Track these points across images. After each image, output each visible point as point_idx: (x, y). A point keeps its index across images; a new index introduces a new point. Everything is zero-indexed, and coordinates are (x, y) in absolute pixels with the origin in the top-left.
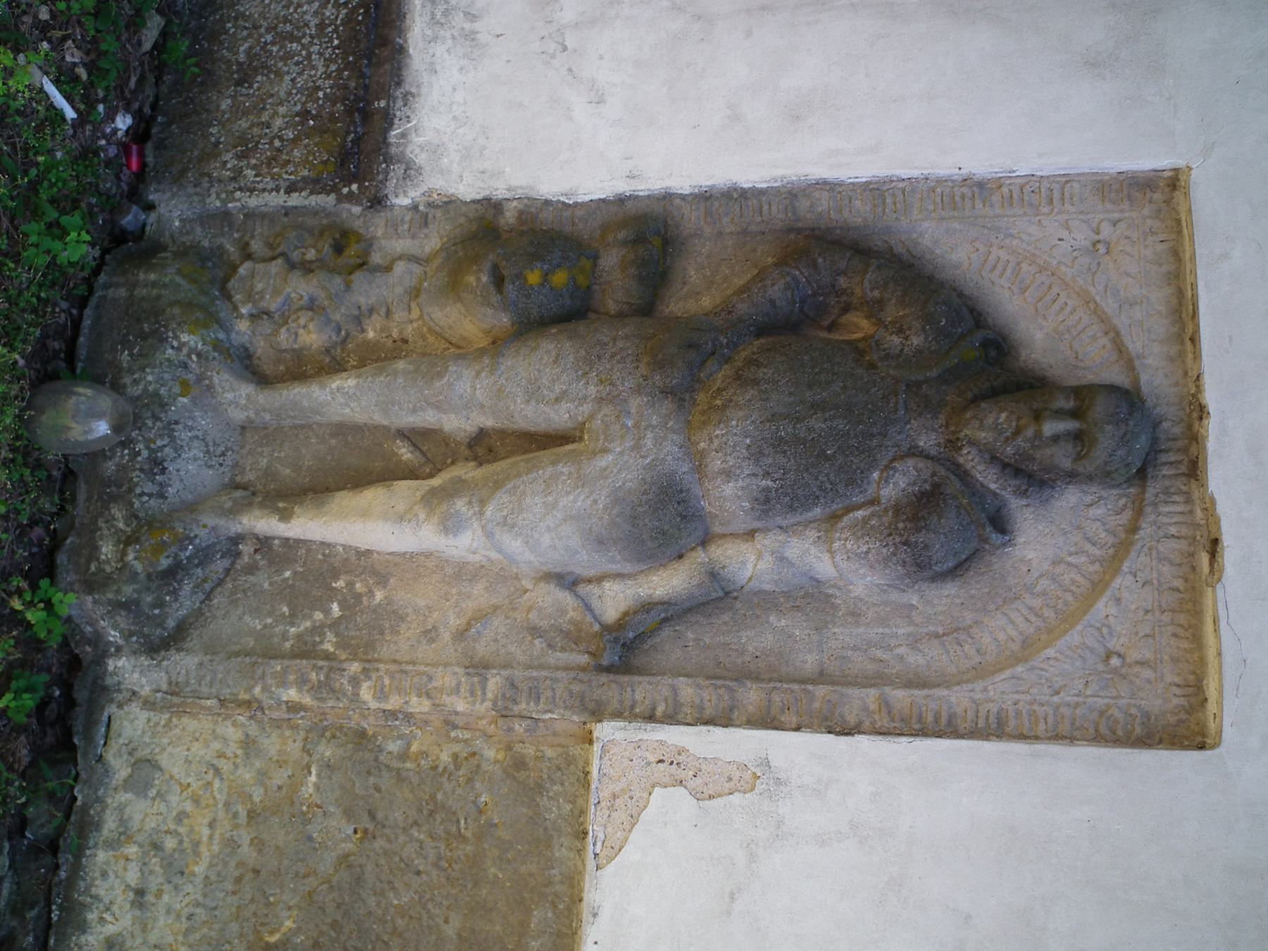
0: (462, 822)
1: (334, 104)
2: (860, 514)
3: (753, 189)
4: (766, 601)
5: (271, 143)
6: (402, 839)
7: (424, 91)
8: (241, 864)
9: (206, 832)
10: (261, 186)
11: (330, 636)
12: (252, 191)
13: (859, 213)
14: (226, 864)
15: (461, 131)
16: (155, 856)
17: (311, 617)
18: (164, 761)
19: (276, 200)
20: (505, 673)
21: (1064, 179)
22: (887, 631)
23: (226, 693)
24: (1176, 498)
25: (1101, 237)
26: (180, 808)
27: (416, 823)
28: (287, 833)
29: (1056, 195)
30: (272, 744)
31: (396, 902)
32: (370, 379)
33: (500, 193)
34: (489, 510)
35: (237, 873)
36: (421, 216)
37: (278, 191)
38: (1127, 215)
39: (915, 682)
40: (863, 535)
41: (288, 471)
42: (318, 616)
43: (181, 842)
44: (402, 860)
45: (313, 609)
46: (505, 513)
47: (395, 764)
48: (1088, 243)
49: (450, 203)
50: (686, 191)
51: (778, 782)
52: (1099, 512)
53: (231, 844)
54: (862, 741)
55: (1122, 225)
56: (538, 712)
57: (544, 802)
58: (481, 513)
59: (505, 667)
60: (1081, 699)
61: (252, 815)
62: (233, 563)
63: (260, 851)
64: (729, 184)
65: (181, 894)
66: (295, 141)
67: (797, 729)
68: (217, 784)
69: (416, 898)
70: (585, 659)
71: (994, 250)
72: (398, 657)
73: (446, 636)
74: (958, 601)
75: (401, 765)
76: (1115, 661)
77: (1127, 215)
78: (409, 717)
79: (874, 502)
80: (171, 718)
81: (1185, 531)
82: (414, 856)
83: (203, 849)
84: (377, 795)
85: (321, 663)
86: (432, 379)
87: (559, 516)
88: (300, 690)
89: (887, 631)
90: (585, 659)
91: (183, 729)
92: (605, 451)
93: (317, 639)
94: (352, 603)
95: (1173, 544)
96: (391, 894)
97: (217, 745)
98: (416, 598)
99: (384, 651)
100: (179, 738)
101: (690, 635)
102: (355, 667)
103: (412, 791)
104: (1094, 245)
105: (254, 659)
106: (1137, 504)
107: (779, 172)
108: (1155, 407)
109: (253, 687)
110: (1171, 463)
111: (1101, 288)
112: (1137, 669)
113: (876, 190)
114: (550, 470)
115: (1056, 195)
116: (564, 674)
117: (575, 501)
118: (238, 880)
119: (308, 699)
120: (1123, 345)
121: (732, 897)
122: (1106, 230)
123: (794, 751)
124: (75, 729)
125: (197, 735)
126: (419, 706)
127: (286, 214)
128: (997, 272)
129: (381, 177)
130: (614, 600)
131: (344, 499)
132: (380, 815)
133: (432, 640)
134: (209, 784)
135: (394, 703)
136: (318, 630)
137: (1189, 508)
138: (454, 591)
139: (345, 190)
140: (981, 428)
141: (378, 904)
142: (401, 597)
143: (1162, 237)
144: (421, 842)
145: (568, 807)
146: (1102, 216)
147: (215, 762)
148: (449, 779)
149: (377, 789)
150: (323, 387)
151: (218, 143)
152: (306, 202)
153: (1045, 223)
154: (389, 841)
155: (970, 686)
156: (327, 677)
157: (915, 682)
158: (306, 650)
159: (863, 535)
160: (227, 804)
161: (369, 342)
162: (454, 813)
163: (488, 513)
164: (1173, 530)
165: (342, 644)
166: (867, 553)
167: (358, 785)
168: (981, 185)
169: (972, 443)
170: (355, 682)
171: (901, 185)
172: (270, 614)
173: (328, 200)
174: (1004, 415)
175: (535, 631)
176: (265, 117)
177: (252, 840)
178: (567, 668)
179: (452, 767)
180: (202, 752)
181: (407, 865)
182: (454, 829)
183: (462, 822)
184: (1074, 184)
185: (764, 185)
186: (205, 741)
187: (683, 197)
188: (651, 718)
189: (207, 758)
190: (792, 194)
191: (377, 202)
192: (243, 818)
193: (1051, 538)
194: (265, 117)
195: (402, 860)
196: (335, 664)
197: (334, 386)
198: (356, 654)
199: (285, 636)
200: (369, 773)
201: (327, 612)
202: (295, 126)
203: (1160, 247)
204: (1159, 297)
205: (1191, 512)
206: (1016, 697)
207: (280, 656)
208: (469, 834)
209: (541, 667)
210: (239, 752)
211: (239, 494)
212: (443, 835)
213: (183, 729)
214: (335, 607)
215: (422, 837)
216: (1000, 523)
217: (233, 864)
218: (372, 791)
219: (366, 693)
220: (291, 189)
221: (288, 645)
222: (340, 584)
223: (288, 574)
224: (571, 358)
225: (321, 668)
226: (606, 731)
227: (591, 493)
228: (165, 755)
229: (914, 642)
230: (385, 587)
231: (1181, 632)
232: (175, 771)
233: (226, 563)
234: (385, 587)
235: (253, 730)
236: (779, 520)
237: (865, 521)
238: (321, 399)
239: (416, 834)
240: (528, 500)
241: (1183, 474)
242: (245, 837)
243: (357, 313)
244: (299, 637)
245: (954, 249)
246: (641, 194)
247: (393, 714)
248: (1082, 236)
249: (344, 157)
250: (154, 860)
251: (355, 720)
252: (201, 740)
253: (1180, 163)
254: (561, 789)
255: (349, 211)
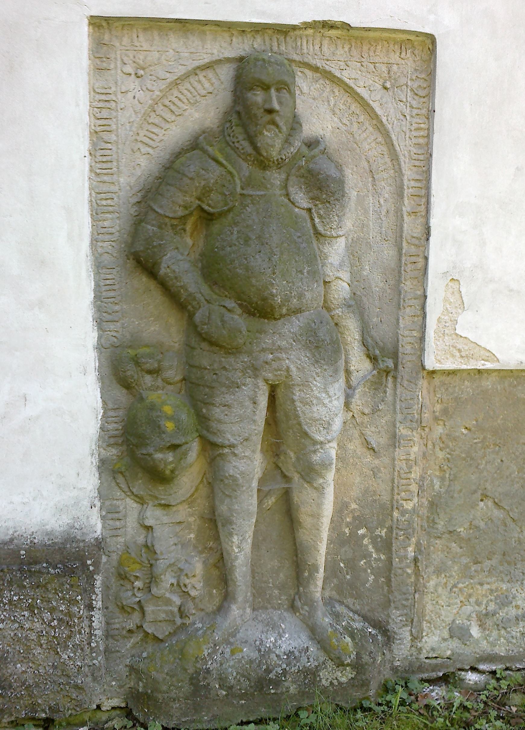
0: (475, 441)
1: (25, 587)
2: (317, 220)
3: (95, 291)
4: (356, 278)
5: (54, 628)
6: (485, 474)
7: (10, 524)
8: (501, 563)
9: (486, 587)
10: (87, 630)
11: (377, 532)
12: (91, 634)
13: (117, 224)
14: (501, 572)
15: (45, 493)
16: (499, 614)
17: (366, 546)
18: (449, 620)
19: (98, 618)
20: (398, 425)
21: (92, 93)
22: (371, 209)
23: (412, 589)
24: (299, 44)
25: (133, 73)
26: (474, 604)
27: (477, 467)
28: (485, 539)
29: (104, 97)
30: (437, 557)
31: (516, 473)
32: (234, 527)
33: (95, 461)
34: (319, 438)
35: (506, 565)
36: (110, 513)
37: (92, 616)
38: (119, 56)
39: (399, 193)
40: (330, 219)
41: (281, 575)
42: (366, 541)
43: (491, 601)
44: (496, 472)
45: (361, 546)
46: (322, 429)
47: (447, 483)
48: (137, 81)
49: (102, 495)
50: (95, 335)
51: (454, 267)
52: (305, 87)
53: (491, 572)
54: (433, 222)
55: (125, 59)
56: (418, 404)
57: (464, 396)
58: (321, 443)
59: (395, 426)
60: (408, 105)
61: (476, 562)
62: (336, 600)
63: (494, 554)
64: (91, 306)
65: (517, 594)
66: (52, 610)
67: (426, 259)
68: (461, 585)
69: (513, 462)
70: (390, 379)
71: (139, 139)
72: (389, 488)
73: (377, 462)
74: (355, 169)
75: (447, 479)
76: (388, 85)
77: (119, 56)
78: (422, 478)
79: (309, 210)
80: (426, 621)
81: (317, 41)
82: (494, 466)
83: (494, 587)
84: (464, 491)
85: (394, 535)
86: (237, 485)
87: (324, 395)
88: (409, 545)
89: (371, 209)
90: (390, 379)
91: (431, 611)
92: (288, 369)
93: (379, 540)
94: (359, 521)
95: (325, 48)
96: (513, 476)
97: (440, 590)
98: (357, 481)
99: (385, 497)
100: (437, 613)
101: (375, 320)
102: (396, 514)
103: (461, 471)
104: (138, 77)
105: (392, 576)
106: (301, 65)
107: (84, 274)
108: (245, 50)
109: (407, 573)
110: (279, 44)
111: (168, 75)
112: (392, 73)
113: (97, 212)
114: (298, 404)
115: (104, 97)
116: (398, 390)
117: (316, 386)
118: (509, 563)
119: (414, 539)
120: (204, 65)
121: (511, 290)
122: (129, 69)
123: (439, 257)
124: (435, 676)
125: (434, 602)
126: (416, 474)
127: (107, 608)
128: (155, 137)
129: (81, 544)
130: (360, 365)
131: (303, 535)
132: (474, 487)
133: (379, 470)
134: (461, 590)
135: (414, 488)
136: (374, 540)
137: (305, 37)
138: (351, 460)
139: (91, 568)
140: (273, 146)
141: (518, 482)
142: (355, 493)
143: (135, 36)
144: (486, 462)
145: (466, 382)
146: (119, 71)
147: (449, 588)
148: (454, 451)
149: (461, 491)
150: (237, 558)
151: (54, 667)
152: (100, 596)
153: (122, 106)
154: (486, 481)
155: (403, 163)
156: (401, 530)
157: (399, 193)
158: (386, 545)
159: (329, 218)
160: (471, 577)
161: (197, 536)
162: (471, 445)
163: (322, 439)
164: (317, 47)
165: (381, 524)
166: (338, 216)
167: (459, 503)
168: (94, 144)
169: (280, 153)
170: (403, 513)
171: (94, 195)
172: (365, 571)
173: (99, 581)
174: (266, 133)
175: (375, 410)
176: (33, 636)
177: (489, 559)
178: (395, 389)
179: (448, 450)
180: (444, 597)
181: (498, 469)
182: (480, 445)
183: (475, 441)
184: (96, 87)
185: (93, 283)
186: (438, 597)
187: (100, 338)
188: (422, 339)
189: (447, 593)
190: (99, 266)
191: (99, 545)
192: (478, 567)
193: (319, 114)
194: (33, 636)
195: (496, 472)
196: (394, 527)
197: (236, 550)
198: (388, 514)
199: (378, 560)
200: (452, 497)
201: (364, 536)
202: (40, 613)
203: (141, 38)
204: (174, 42)
205: (307, 36)
206: (407, 139)
207: (390, 560)
208: (482, 436)
209: (394, 404)
210: (443, 575)
211: (298, 604)
212: (483, 450)
213: (431, 611)
214: (361, 532)
215: (484, 462)
216: (312, 143)
217: (501, 568)
218: (461, 494)
219: (409, 506)
220: (90, 607)
221: (383, 557)
222: (347, 531)
223: (342, 565)
224: (227, 396)
225: (397, 534)
226: (430, 363)
227: (312, 376)
228: (447, 619)
229: (377, 193)
230: (349, 503)
231: (372, 48)
232: (455, 611)
233: (337, 605)
234: (349, 503)
235: (431, 569)
236: (320, 267)
237: (320, 217)
238: (243, 559)
239: (483, 466)
240: (315, 415)
241: (285, 38)
242: (488, 563)
243: (180, 546)
244: (378, 550)
245: (136, 167)
246: (97, 364)
247: (420, 487)
248: (132, 84)
249: (69, 572)
250: (501, 614)
251: (424, 512)
252: (437, 599)
253: (86, 21)
254: (457, 388)
255: (105, 563)
